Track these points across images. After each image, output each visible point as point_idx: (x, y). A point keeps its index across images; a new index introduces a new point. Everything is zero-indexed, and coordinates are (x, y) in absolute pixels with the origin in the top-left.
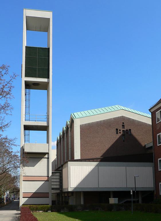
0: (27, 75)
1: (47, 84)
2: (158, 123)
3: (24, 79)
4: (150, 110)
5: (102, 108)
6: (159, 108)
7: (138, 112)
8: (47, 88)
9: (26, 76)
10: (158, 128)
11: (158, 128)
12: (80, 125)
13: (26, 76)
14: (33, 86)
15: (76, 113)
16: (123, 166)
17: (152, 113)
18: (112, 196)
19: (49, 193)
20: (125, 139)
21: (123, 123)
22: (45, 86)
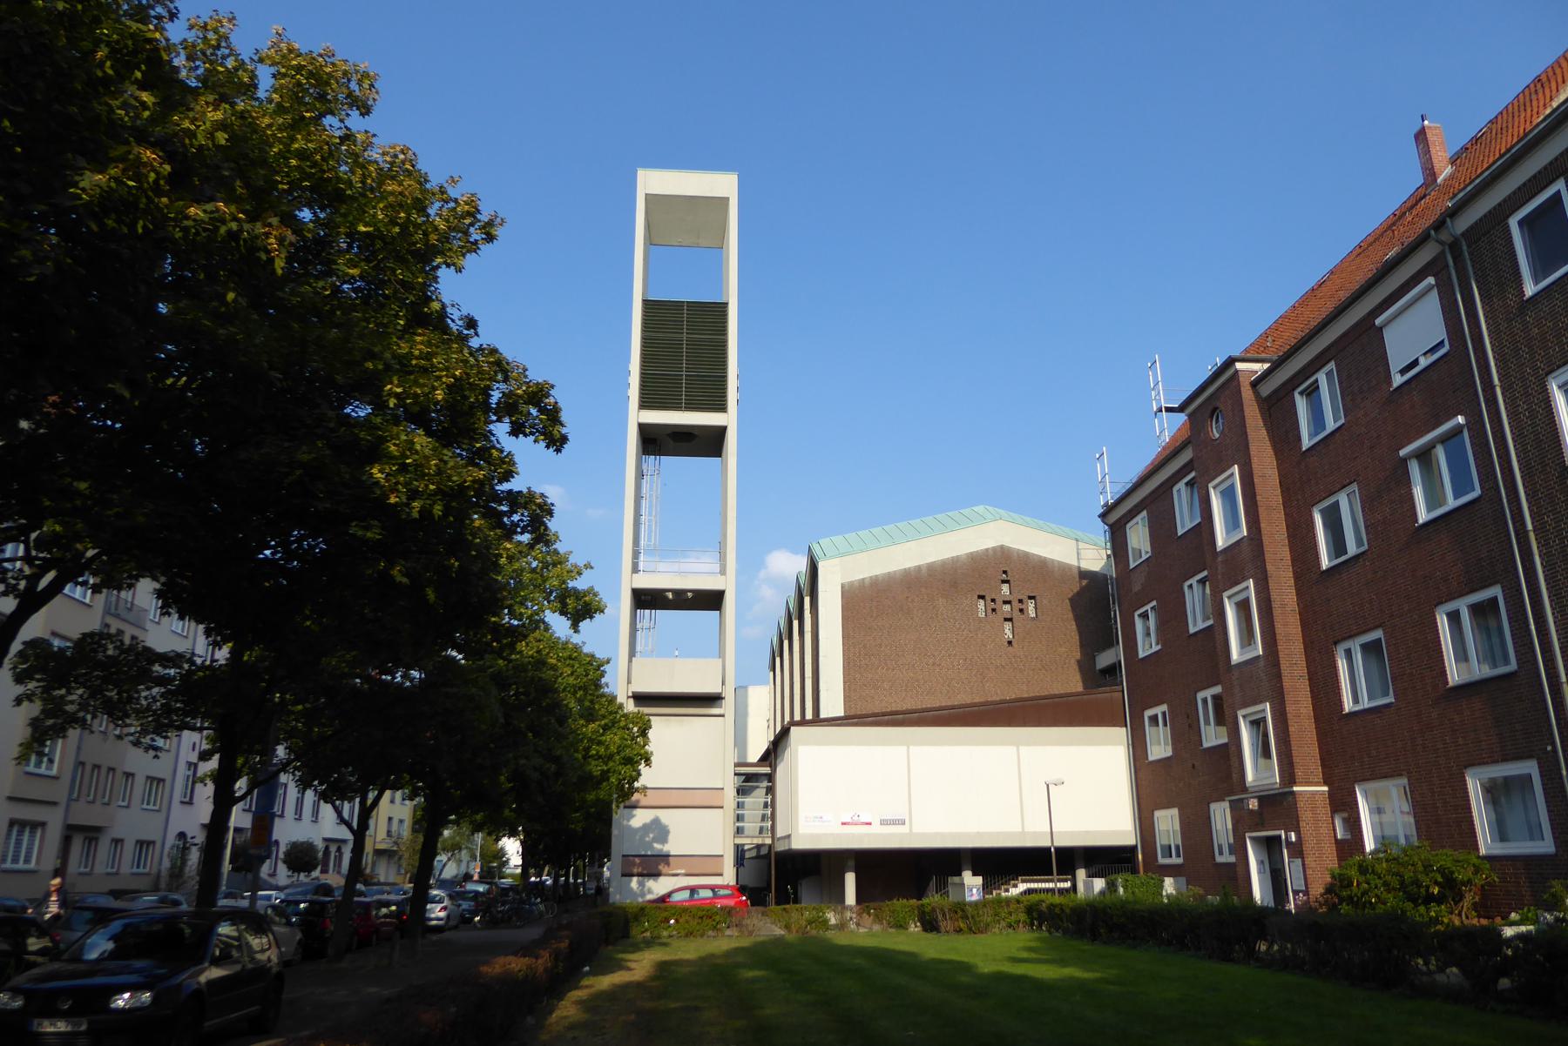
0: (649, 400)
1: (721, 432)
2: (1136, 564)
3: (638, 417)
4: (1103, 516)
5: (939, 516)
6: (1136, 506)
7: (1064, 529)
8: (1473, 609)
9: (646, 404)
10: (1137, 588)
11: (1137, 588)
12: (843, 586)
13: (646, 404)
14: (672, 442)
15: (841, 537)
16: (797, 751)
17: (1111, 526)
18: (1345, 815)
19: (722, 856)
20: (1013, 637)
21: (1005, 572)
22: (710, 443)
